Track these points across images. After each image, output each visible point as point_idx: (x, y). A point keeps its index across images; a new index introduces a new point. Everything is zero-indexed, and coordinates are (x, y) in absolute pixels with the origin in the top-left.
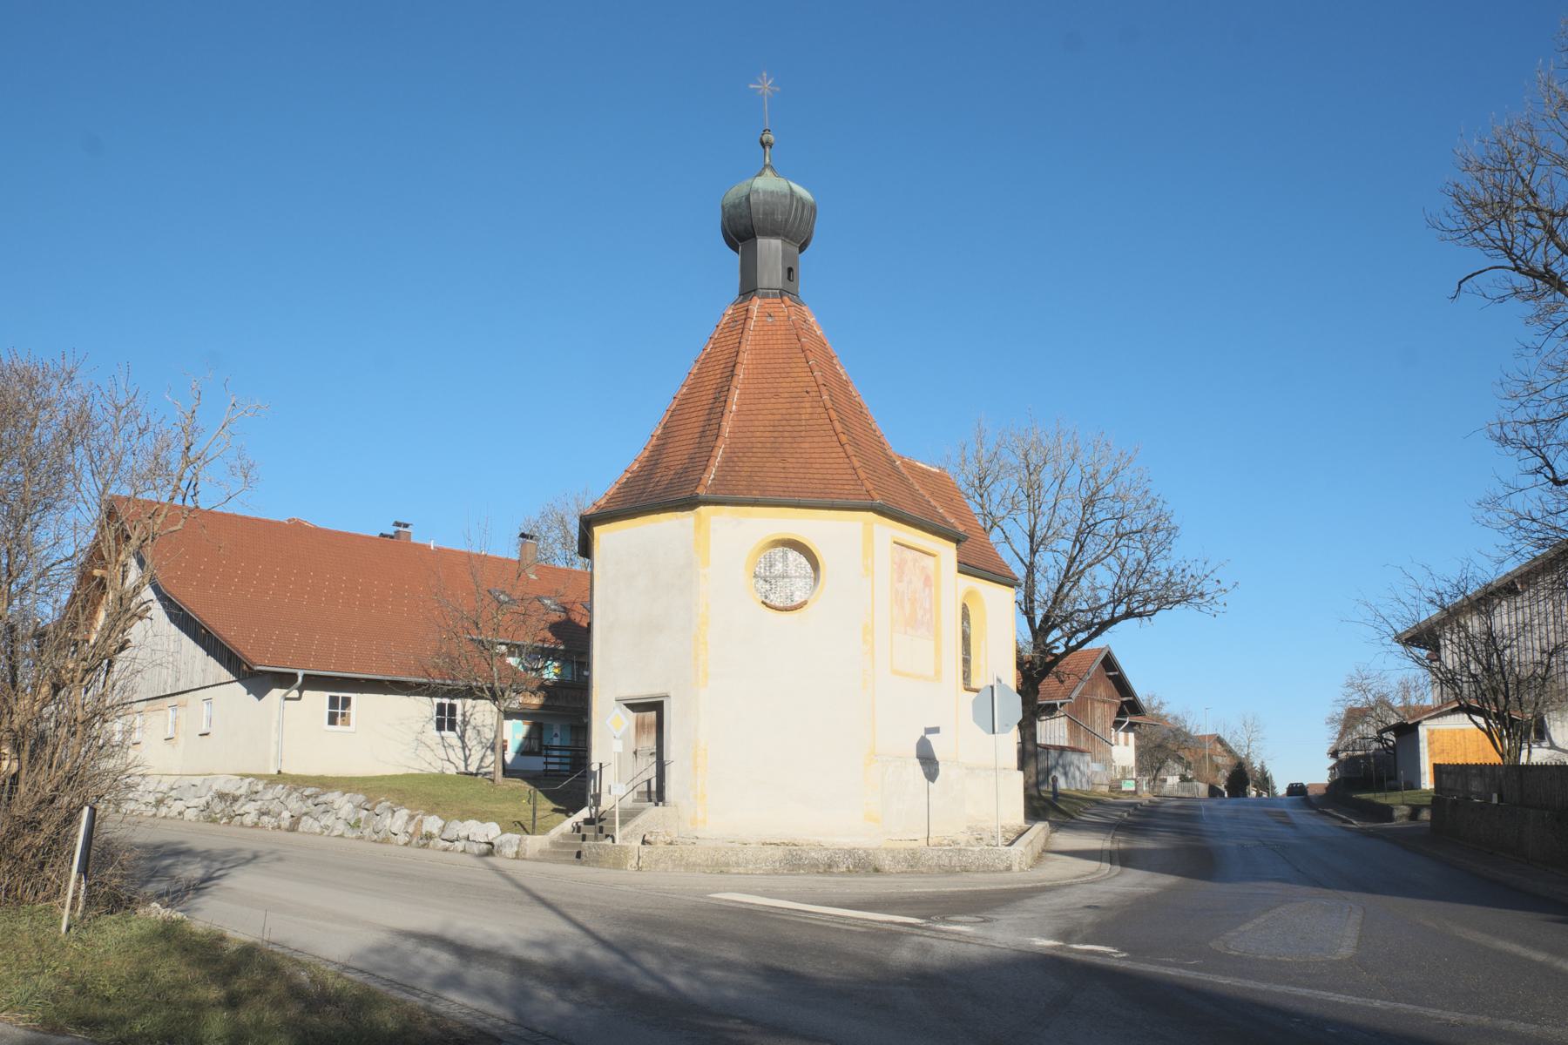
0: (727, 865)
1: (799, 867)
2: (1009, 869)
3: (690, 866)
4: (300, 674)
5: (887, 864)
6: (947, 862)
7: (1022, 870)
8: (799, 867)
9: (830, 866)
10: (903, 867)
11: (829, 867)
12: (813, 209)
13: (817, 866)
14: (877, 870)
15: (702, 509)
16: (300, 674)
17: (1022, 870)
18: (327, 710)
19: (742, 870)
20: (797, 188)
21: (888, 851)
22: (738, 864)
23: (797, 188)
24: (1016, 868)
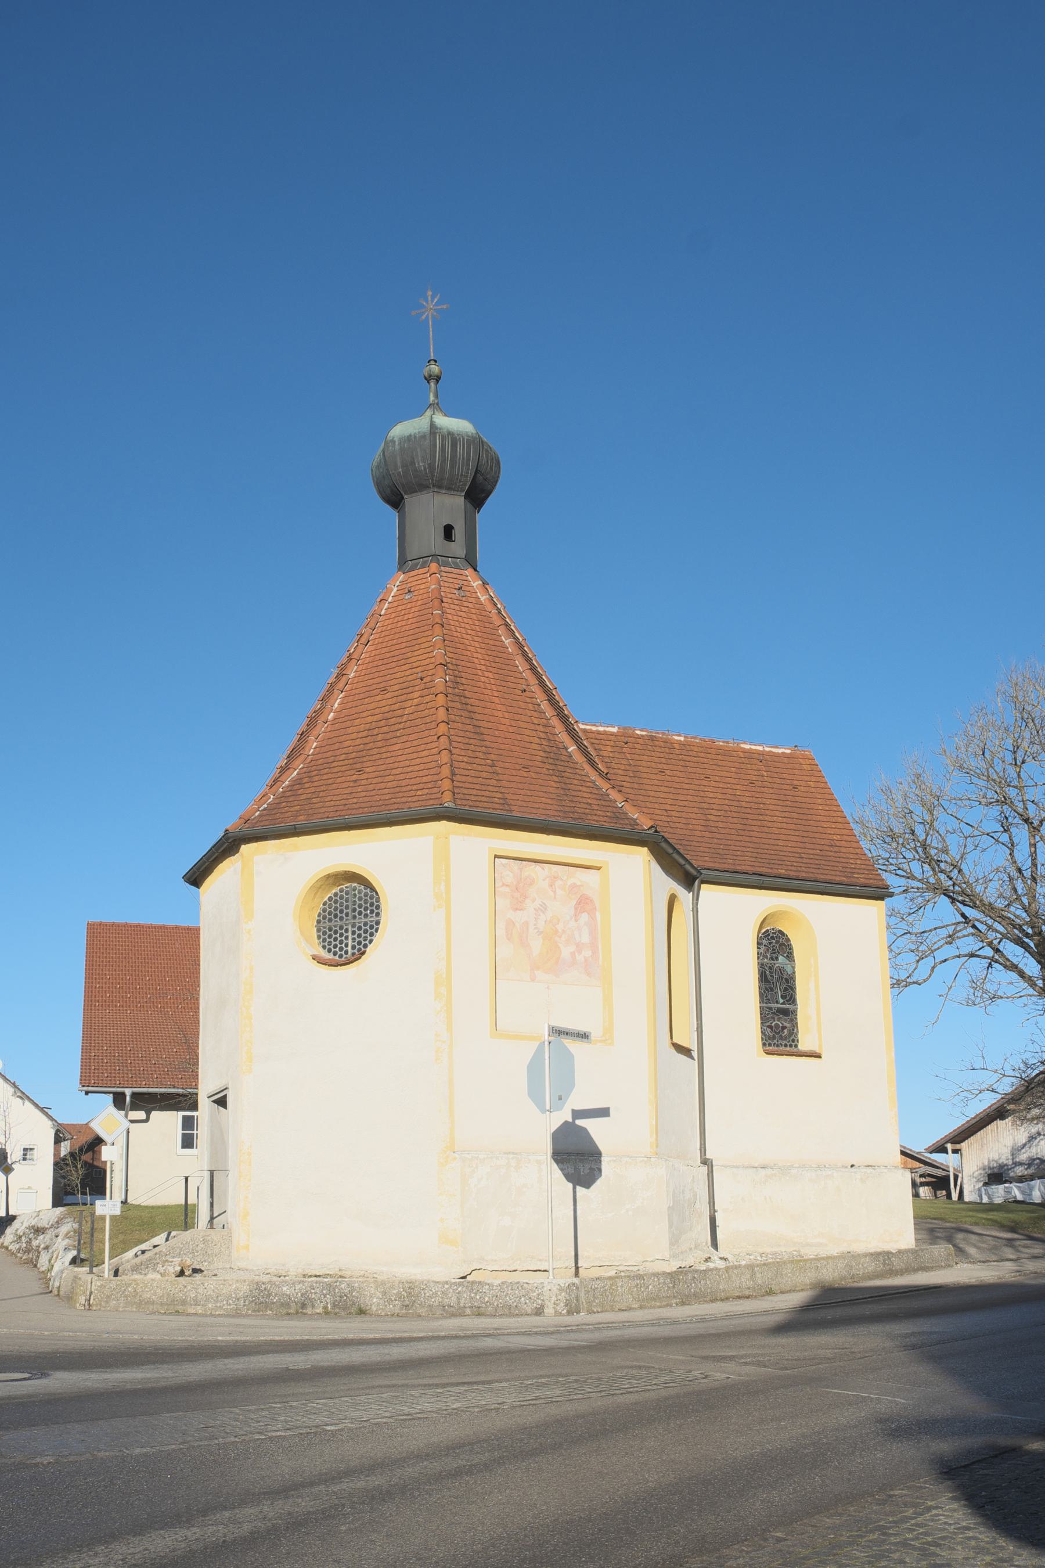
0: (184, 1302)
1: (267, 1306)
2: (539, 1312)
3: (143, 1304)
4: (128, 1092)
5: (374, 1302)
6: (453, 1301)
7: (558, 1314)
8: (267, 1306)
9: (304, 1306)
10: (395, 1307)
11: (301, 1308)
12: (476, 443)
13: (287, 1305)
14: (362, 1312)
15: (244, 848)
16: (128, 1092)
17: (558, 1314)
18: (180, 1132)
19: (199, 1310)
20: (443, 421)
21: (379, 1284)
22: (197, 1303)
23: (443, 421)
24: (549, 1310)
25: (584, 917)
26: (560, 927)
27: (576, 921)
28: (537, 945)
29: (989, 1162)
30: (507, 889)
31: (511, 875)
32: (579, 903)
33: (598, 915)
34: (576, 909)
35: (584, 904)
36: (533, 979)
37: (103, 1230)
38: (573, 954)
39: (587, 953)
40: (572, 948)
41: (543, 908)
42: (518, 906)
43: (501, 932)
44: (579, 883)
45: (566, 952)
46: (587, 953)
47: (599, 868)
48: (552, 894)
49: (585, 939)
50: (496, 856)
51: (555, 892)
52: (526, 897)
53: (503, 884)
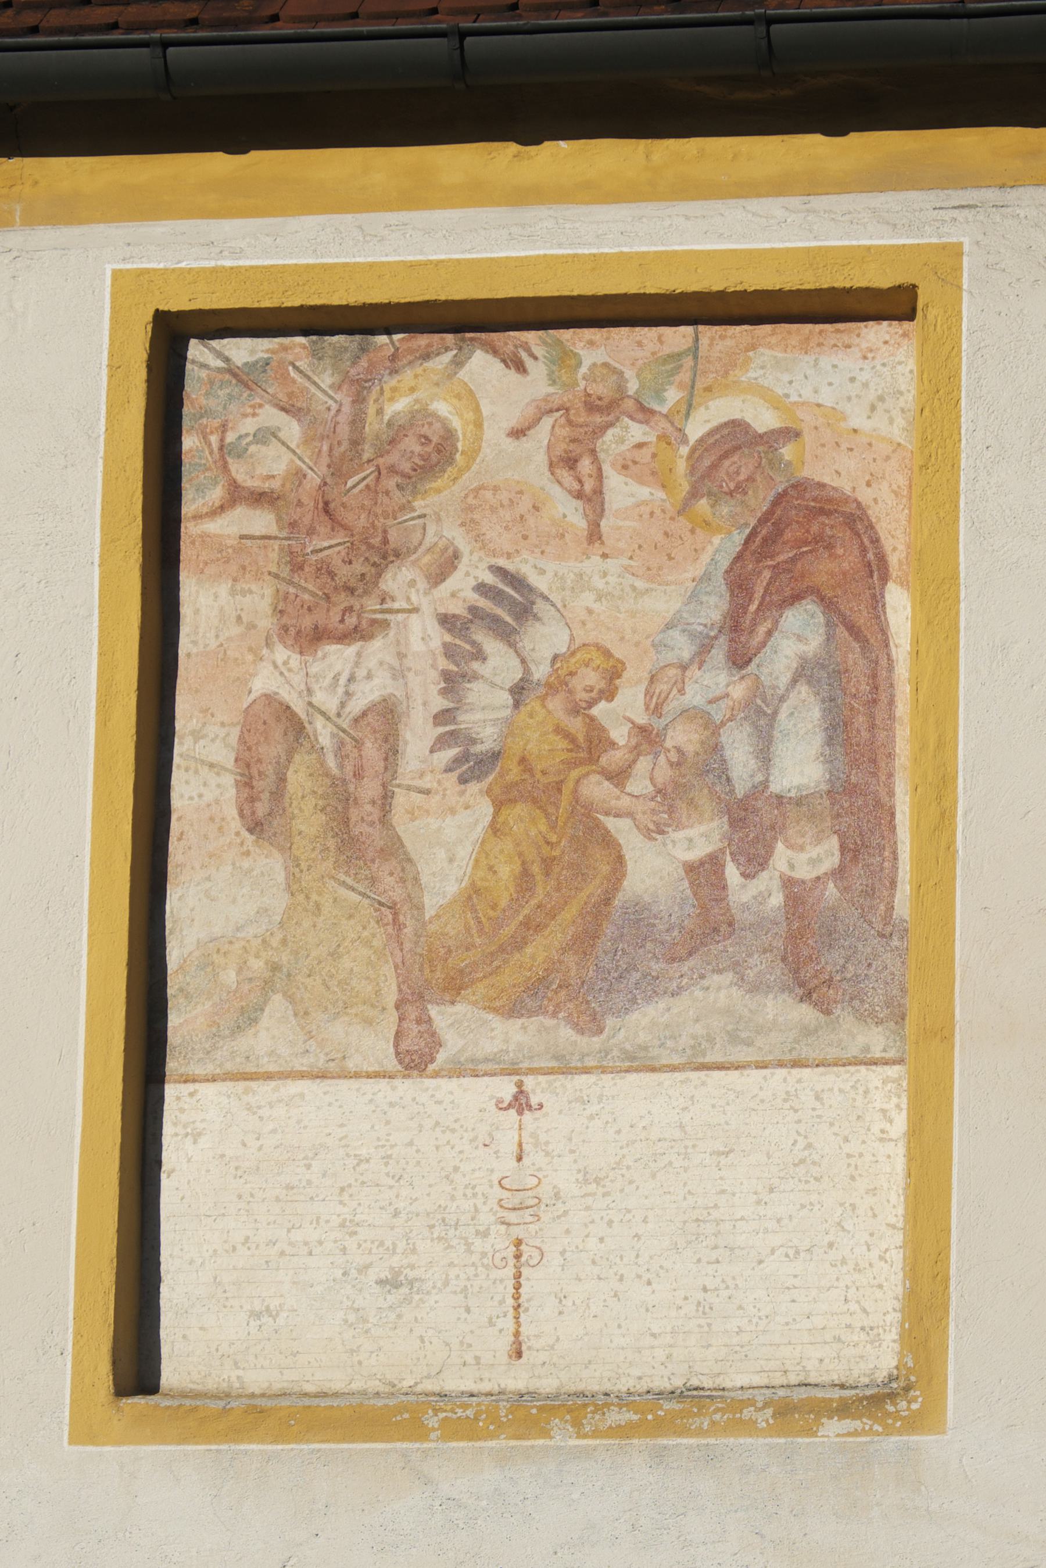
25: (798, 634)
26: (621, 713)
27: (740, 660)
28: (448, 840)
29: (349, 396)
30: (261, 521)
31: (292, 430)
32: (763, 541)
33: (899, 606)
34: (739, 585)
35: (800, 547)
36: (416, 1059)
37: (548, 18)
38: (705, 874)
39: (807, 856)
40: (700, 837)
41: (511, 603)
42: (331, 607)
43: (199, 789)
44: (764, 419)
45: (654, 868)
46: (807, 856)
47: (896, 305)
48: (573, 514)
49: (800, 764)
50: (137, 1365)
51: (593, 499)
52: (387, 555)
53: (238, 495)
